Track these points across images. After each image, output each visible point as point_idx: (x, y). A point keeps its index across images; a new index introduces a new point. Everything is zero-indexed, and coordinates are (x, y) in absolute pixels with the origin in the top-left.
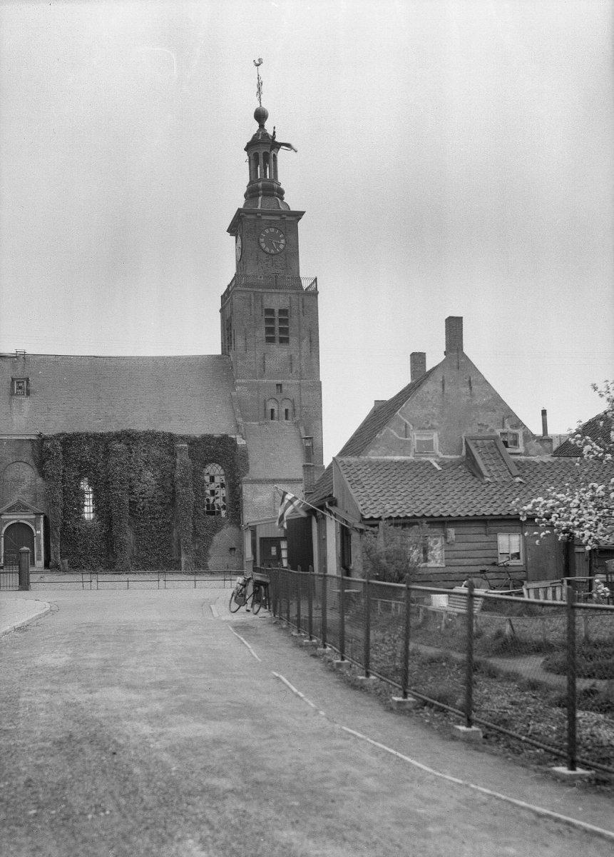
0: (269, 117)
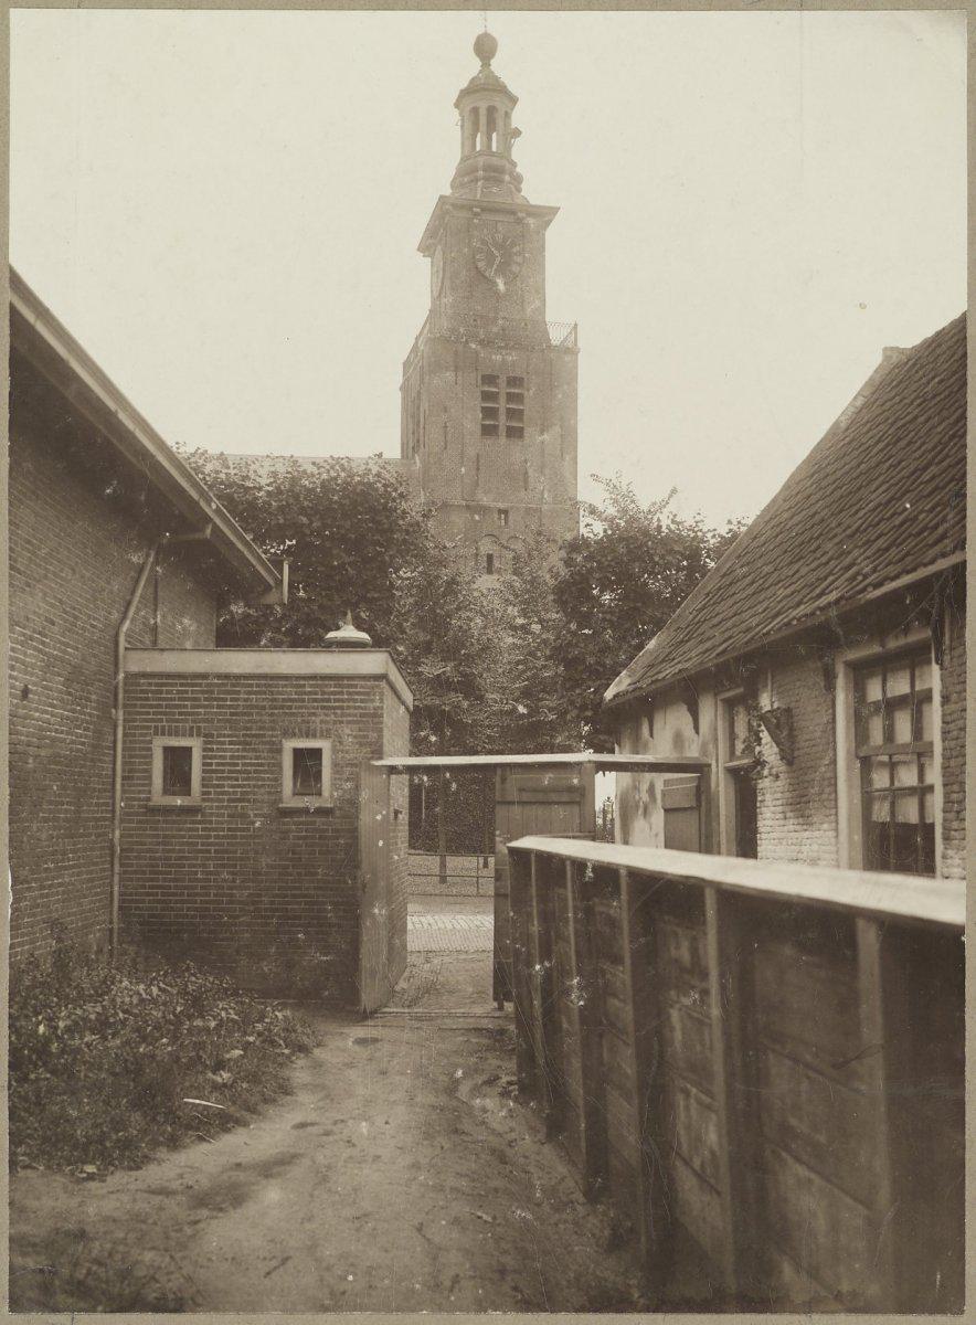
0: (420, 218)
